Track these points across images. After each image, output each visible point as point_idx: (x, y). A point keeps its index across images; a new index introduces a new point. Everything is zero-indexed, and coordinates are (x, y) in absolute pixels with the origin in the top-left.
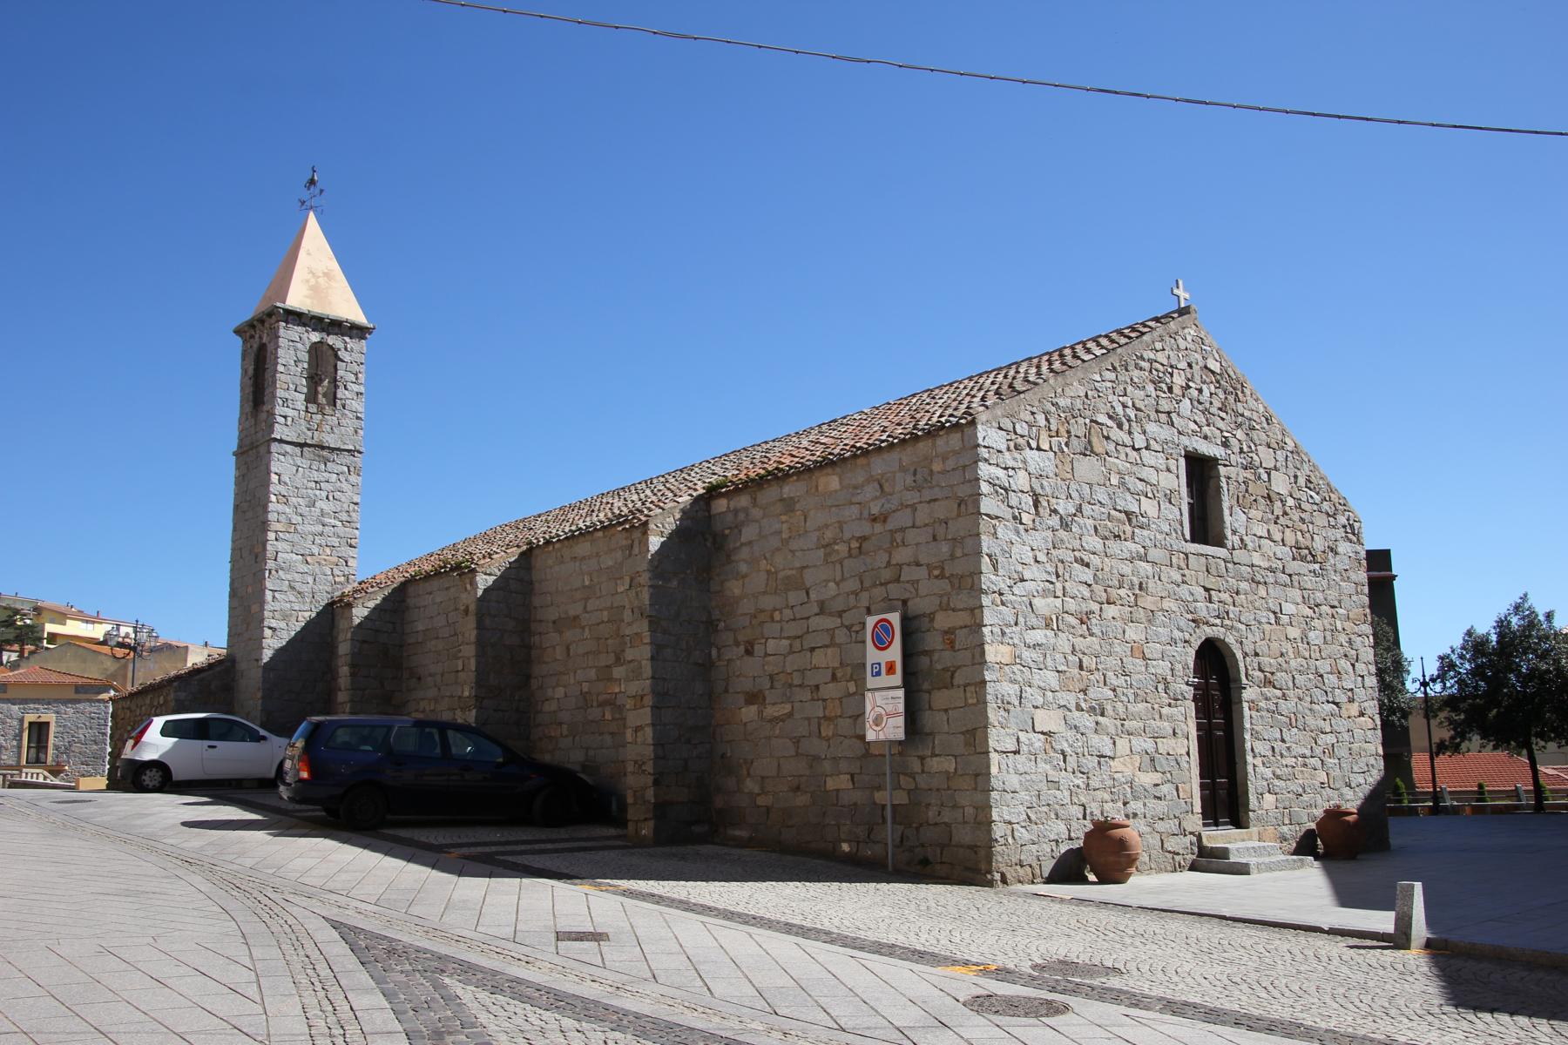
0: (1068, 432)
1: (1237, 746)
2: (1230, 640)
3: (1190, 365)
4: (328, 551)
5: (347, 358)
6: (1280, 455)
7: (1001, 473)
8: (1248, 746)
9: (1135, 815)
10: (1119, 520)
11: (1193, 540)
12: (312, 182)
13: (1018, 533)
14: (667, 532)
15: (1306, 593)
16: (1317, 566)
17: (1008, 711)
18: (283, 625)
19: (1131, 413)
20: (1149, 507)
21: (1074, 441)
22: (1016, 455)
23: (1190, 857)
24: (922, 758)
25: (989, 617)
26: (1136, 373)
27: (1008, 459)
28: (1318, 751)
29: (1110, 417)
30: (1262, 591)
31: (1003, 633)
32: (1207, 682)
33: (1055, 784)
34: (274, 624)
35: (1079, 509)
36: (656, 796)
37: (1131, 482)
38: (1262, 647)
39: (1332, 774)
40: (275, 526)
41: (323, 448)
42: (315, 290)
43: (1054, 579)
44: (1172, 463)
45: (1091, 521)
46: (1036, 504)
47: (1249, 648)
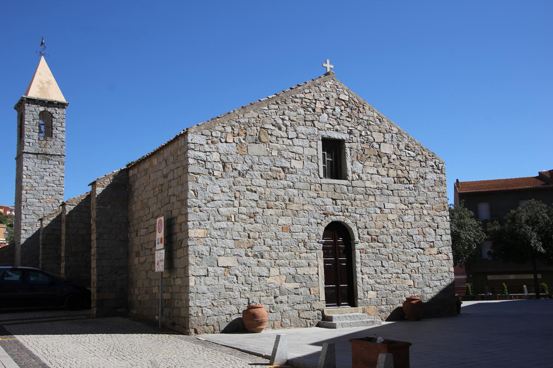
0: (246, 134)
1: (354, 269)
2: (348, 222)
3: (328, 98)
4: (50, 197)
5: (57, 117)
6: (388, 136)
7: (202, 155)
8: (358, 269)
9: (281, 302)
10: (277, 171)
12: (42, 43)
13: (211, 180)
17: (202, 258)
18: (30, 228)
19: (288, 123)
20: (297, 164)
21: (249, 138)
22: (212, 146)
23: (317, 321)
24: (174, 279)
25: (190, 217)
26: (291, 105)
28: (407, 271)
29: (273, 125)
30: (372, 199)
31: (200, 224)
32: (335, 241)
33: (231, 290)
34: (26, 228)
35: (251, 167)
36: (97, 296)
37: (285, 154)
38: (370, 224)
39: (417, 281)
41: (47, 155)
42: (42, 89)
43: (233, 199)
44: (313, 144)
45: (259, 172)
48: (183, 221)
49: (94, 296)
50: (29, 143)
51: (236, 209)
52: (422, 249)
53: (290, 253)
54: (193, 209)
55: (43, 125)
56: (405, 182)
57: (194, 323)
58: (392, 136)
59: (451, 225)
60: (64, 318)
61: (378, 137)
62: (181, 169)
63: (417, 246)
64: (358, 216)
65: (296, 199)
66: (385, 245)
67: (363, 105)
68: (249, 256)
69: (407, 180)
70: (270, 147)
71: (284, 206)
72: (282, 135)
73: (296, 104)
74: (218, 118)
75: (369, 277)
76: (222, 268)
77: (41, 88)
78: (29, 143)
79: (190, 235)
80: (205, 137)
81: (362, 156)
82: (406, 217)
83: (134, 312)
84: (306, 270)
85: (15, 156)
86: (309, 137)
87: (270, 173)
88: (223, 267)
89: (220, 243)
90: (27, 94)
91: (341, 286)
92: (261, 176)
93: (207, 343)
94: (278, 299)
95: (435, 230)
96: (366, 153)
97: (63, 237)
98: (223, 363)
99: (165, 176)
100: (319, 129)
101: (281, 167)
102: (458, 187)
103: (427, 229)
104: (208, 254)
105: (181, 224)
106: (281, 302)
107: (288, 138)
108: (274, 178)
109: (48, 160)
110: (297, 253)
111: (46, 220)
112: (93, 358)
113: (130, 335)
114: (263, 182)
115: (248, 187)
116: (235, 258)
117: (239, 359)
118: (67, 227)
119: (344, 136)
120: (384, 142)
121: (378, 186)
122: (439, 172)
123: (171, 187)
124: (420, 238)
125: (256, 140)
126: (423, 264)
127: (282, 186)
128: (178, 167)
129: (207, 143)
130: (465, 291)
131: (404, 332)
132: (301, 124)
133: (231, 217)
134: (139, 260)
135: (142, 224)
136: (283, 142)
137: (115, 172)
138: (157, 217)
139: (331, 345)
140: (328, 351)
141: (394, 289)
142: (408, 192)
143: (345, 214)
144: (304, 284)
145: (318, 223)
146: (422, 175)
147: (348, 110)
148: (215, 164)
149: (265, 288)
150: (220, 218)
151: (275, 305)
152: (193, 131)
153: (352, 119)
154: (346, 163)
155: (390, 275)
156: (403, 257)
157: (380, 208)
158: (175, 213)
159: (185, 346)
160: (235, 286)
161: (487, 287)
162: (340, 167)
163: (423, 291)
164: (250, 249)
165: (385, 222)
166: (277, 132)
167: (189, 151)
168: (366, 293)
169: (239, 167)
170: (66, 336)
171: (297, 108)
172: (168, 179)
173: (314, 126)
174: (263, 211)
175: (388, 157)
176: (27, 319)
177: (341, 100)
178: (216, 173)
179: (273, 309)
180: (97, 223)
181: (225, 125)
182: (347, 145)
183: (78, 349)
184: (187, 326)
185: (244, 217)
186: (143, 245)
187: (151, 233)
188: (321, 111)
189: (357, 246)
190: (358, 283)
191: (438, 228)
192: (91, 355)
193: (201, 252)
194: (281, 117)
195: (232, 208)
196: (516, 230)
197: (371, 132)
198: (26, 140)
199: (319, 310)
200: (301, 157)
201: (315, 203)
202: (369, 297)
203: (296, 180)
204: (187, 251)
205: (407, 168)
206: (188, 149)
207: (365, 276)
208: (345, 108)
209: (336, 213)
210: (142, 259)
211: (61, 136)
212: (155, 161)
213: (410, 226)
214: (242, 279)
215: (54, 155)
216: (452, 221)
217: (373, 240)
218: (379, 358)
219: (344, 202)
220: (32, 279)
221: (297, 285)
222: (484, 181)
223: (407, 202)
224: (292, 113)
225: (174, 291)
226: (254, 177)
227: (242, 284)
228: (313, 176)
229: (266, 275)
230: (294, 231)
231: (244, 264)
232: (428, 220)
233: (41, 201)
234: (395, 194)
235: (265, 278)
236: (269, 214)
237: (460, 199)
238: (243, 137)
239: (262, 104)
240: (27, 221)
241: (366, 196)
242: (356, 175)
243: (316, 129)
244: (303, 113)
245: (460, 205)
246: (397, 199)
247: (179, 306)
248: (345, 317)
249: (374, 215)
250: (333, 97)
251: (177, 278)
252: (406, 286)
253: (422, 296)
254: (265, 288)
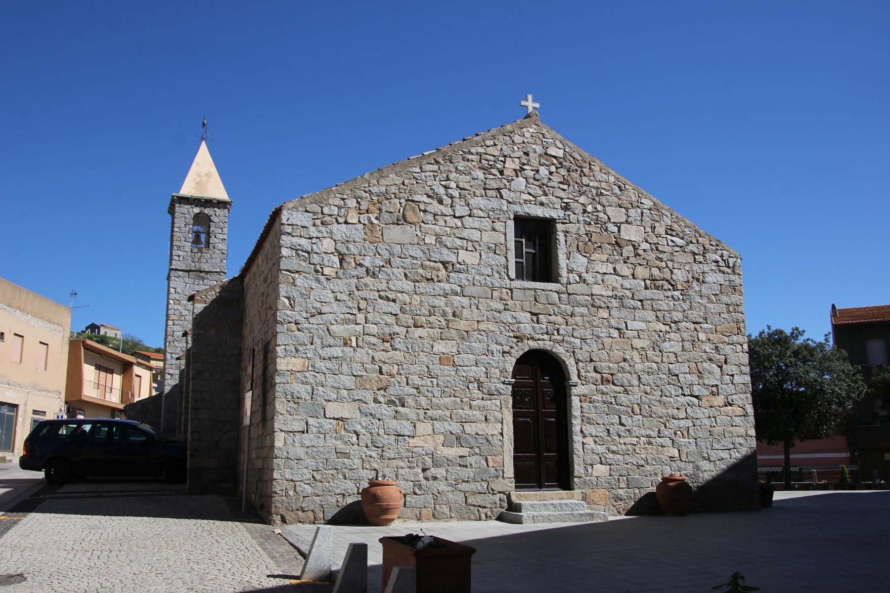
2: (560, 350)
5: (216, 220)
9: (435, 478)
11: (520, 276)
16: (677, 294)
27: (313, 232)
29: (429, 196)
31: (297, 350)
34: (171, 371)
41: (201, 272)
42: (199, 184)
43: (355, 311)
44: (499, 226)
46: (342, 261)
53: (453, 398)
65: (465, 313)
75: (595, 442)
84: (481, 428)
145: (504, 352)
189: (574, 390)
207: (589, 440)
209: (537, 336)
230: (461, 364)
249: (607, 341)
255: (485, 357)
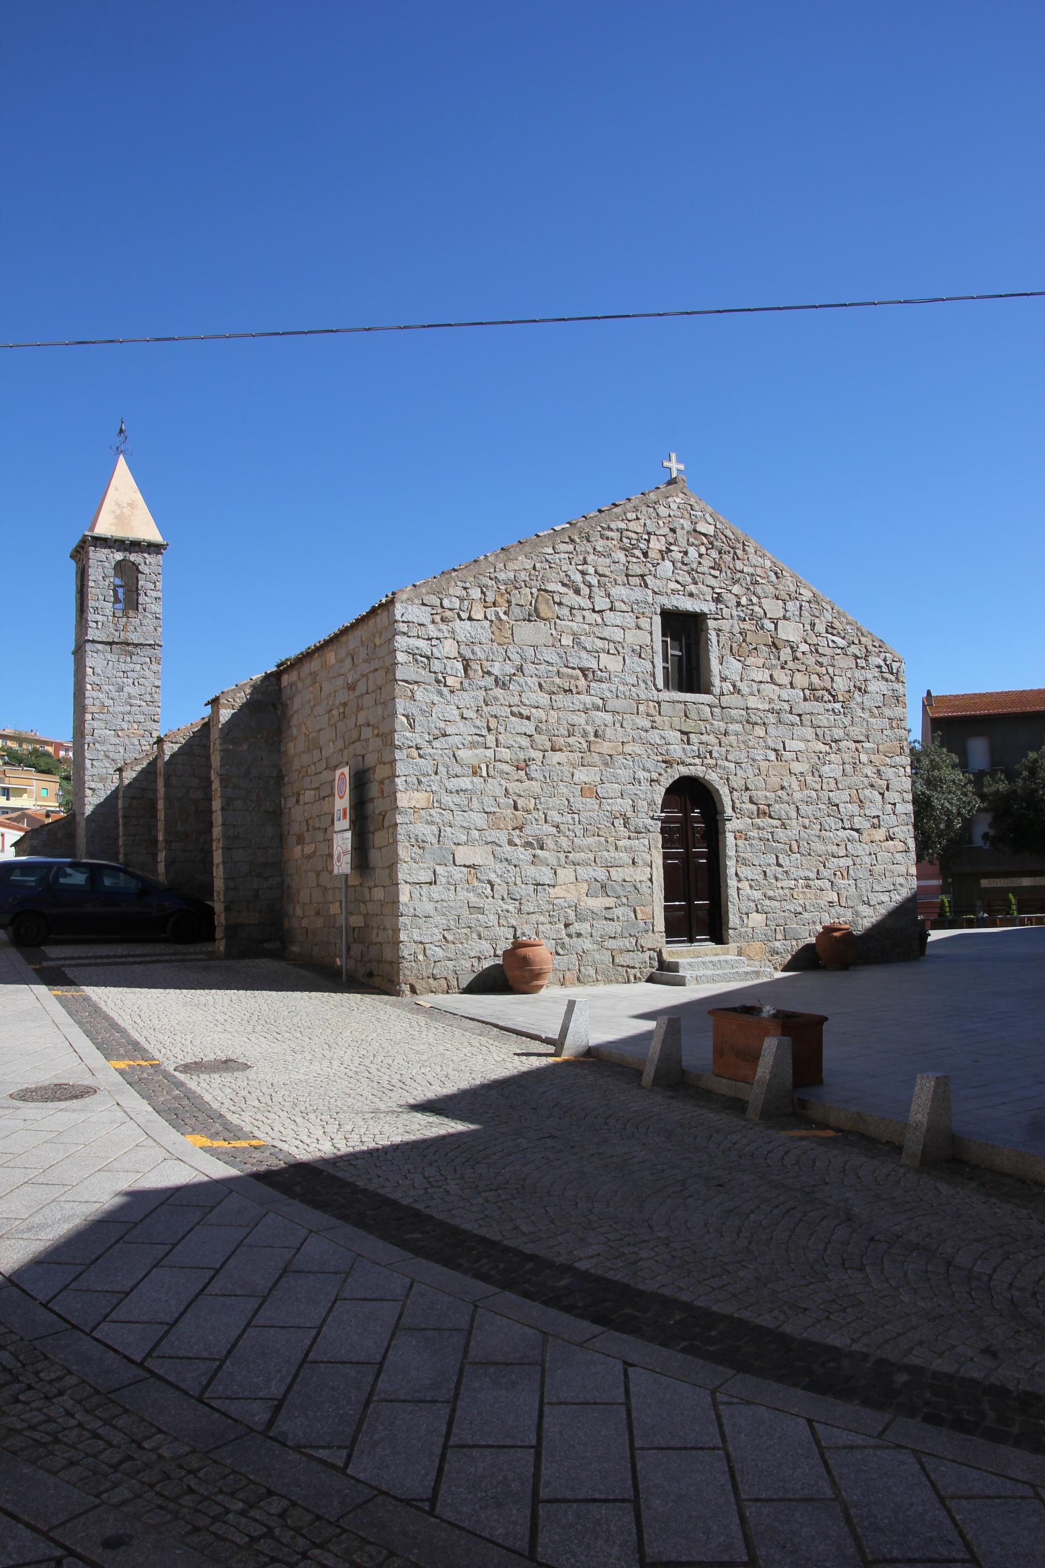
0: (509, 602)
2: (713, 777)
4: (135, 726)
5: (147, 571)
7: (422, 644)
8: (731, 871)
9: (579, 935)
10: (572, 677)
14: (237, 706)
15: (819, 731)
17: (423, 848)
18: (100, 785)
21: (516, 610)
22: (443, 627)
24: (370, 888)
25: (400, 768)
26: (600, 544)
27: (432, 631)
28: (826, 873)
29: (564, 585)
30: (760, 731)
31: (420, 782)
32: (686, 815)
33: (481, 910)
34: (93, 785)
35: (521, 669)
37: (587, 642)
39: (844, 893)
40: (91, 709)
41: (128, 644)
42: (120, 519)
43: (484, 732)
44: (644, 622)
45: (535, 679)
46: (466, 668)
47: (737, 782)
48: (386, 775)
49: (220, 919)
50: (96, 622)
51: (490, 753)
52: (857, 830)
54: (405, 751)
55: (121, 586)
56: (826, 699)
57: (409, 973)
58: (801, 606)
59: (914, 783)
60: (166, 958)
61: (774, 608)
62: (381, 673)
63: (847, 825)
64: (732, 765)
65: (609, 732)
66: (783, 824)
67: (744, 544)
68: (516, 845)
69: (830, 694)
70: (558, 628)
71: (585, 745)
72: (582, 605)
73: (609, 543)
74: (455, 570)
75: (751, 887)
76: (462, 868)
77: (117, 517)
78: (96, 622)
79: (400, 804)
80: (429, 608)
81: (740, 646)
82: (826, 768)
83: (295, 949)
84: (628, 873)
85: (73, 648)
86: (634, 609)
87: (557, 680)
88: (465, 866)
89: (459, 819)
90: (92, 529)
91: (697, 903)
92: (540, 685)
93: (434, 1012)
94: (572, 930)
95: (882, 794)
96: (748, 640)
97: (161, 805)
98: (466, 1051)
99: (352, 687)
100: (655, 593)
101: (580, 669)
102: (930, 705)
103: (867, 792)
104: (435, 841)
105: (382, 782)
106: (579, 935)
107: (594, 611)
108: (565, 691)
109: (131, 655)
110: (610, 839)
111: (129, 770)
112: (222, 1036)
113: (289, 993)
114: (543, 699)
115: (514, 709)
116: (489, 848)
117: (496, 1043)
118: (167, 785)
119: (705, 606)
120: (785, 618)
121: (772, 705)
122: (893, 678)
123: (362, 709)
124: (853, 808)
125: (529, 615)
126: (858, 861)
127: (581, 707)
128: (376, 670)
129: (433, 622)
130: (938, 910)
131: (815, 995)
132: (619, 581)
133: (480, 768)
134: (303, 850)
135: (308, 779)
136: (584, 617)
137: (254, 678)
138: (336, 767)
139: (674, 1019)
140: (666, 1032)
141: (800, 909)
142: (832, 718)
143: (706, 761)
144: (624, 900)
145: (652, 781)
146: (858, 684)
147: (714, 554)
148: (449, 663)
149: (547, 907)
150: (458, 770)
151: (567, 940)
152: (404, 597)
153: (721, 571)
154: (709, 660)
155: (793, 882)
156: (819, 847)
157: (775, 750)
158: (371, 760)
159: (392, 1017)
160: (488, 904)
161: (979, 903)
162: (698, 668)
163: (857, 913)
164: (517, 831)
165: (785, 778)
166: (571, 598)
167: (397, 637)
168: (745, 916)
169: (496, 670)
170: (172, 991)
171: (610, 549)
172: (357, 693)
173: (646, 586)
174: (544, 756)
175: (792, 648)
176: (101, 957)
177: (700, 533)
178: (450, 681)
179: (563, 947)
180: (224, 780)
181: (468, 585)
182: (711, 623)
183: (194, 1017)
184: (396, 979)
185: (506, 768)
186: (310, 822)
187: (324, 798)
188: (660, 556)
189: (729, 826)
190: (730, 898)
191: (888, 789)
192: (218, 1029)
193: (421, 837)
194: (580, 567)
195: (482, 750)
196: (1037, 791)
197: (759, 597)
198: (91, 616)
199: (653, 950)
200: (620, 649)
201: (652, 739)
202: (751, 924)
203: (609, 695)
204: (395, 834)
205: (831, 670)
206: (396, 633)
207: (744, 885)
208: (707, 549)
210: (309, 849)
211: (155, 608)
212: (331, 657)
213: (833, 786)
214: (501, 890)
215: (141, 644)
216: (916, 774)
217: (760, 814)
218: (765, 1045)
219: (705, 738)
220: (108, 882)
221: (610, 902)
222: (980, 694)
223: (828, 738)
224: (602, 560)
225: (370, 912)
226: (526, 689)
227: (503, 899)
228: (643, 685)
229: (548, 882)
231: (507, 860)
232: (869, 774)
233: (120, 733)
234: (805, 722)
235: (547, 887)
236: (555, 763)
237: (934, 731)
238: (504, 609)
239: (541, 542)
240: (95, 771)
241: (748, 727)
242: (729, 685)
243: (650, 592)
244: (623, 559)
245: (933, 742)
246: (809, 733)
247: (379, 940)
248: (703, 963)
249: (764, 765)
250: (683, 528)
251: (376, 886)
252: (823, 903)
253: (854, 923)
254: (547, 907)
255: (631, 786)
